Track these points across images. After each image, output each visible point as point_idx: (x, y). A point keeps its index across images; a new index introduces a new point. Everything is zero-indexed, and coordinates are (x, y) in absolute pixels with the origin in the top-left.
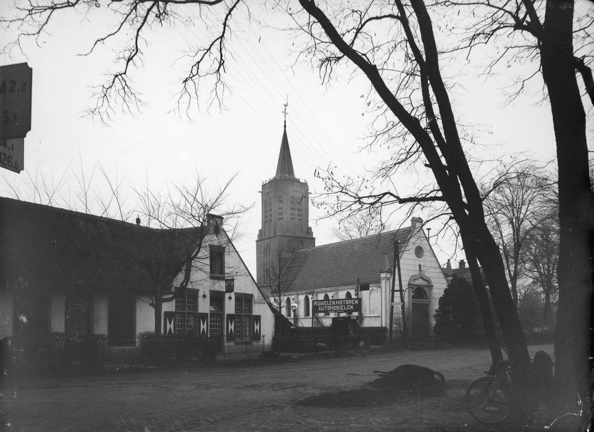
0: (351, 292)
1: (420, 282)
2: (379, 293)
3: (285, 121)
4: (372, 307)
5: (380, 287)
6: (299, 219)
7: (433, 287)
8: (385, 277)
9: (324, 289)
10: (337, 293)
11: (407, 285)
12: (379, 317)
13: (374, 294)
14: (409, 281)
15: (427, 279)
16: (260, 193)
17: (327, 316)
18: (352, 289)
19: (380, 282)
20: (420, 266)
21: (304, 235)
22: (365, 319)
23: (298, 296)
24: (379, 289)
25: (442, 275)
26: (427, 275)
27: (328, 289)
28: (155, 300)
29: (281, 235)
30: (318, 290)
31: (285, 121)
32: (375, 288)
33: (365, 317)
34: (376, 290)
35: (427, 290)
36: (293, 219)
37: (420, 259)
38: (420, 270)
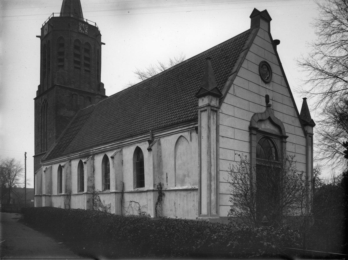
0: (140, 147)
1: (267, 127)
2: (195, 144)
3: (167, 182)
4: (180, 172)
5: (196, 129)
6: (85, 70)
7: (287, 140)
8: (209, 105)
9: (102, 147)
10: (121, 151)
11: (247, 129)
12: (197, 190)
13: (183, 146)
14: (251, 122)
15: (279, 124)
16: (39, 39)
17: (107, 191)
18: (144, 141)
19: (195, 120)
20: (267, 97)
21: (92, 91)
22: (167, 194)
23: (70, 162)
24: (194, 134)
25: (297, 123)
26: (278, 116)
27: (108, 146)
28: (256, 217)
29: (60, 86)
30: (95, 149)
31: (167, 182)
32: (186, 134)
33: (166, 191)
34: (189, 139)
35: (278, 143)
36: (78, 68)
37: (267, 86)
38: (268, 106)
